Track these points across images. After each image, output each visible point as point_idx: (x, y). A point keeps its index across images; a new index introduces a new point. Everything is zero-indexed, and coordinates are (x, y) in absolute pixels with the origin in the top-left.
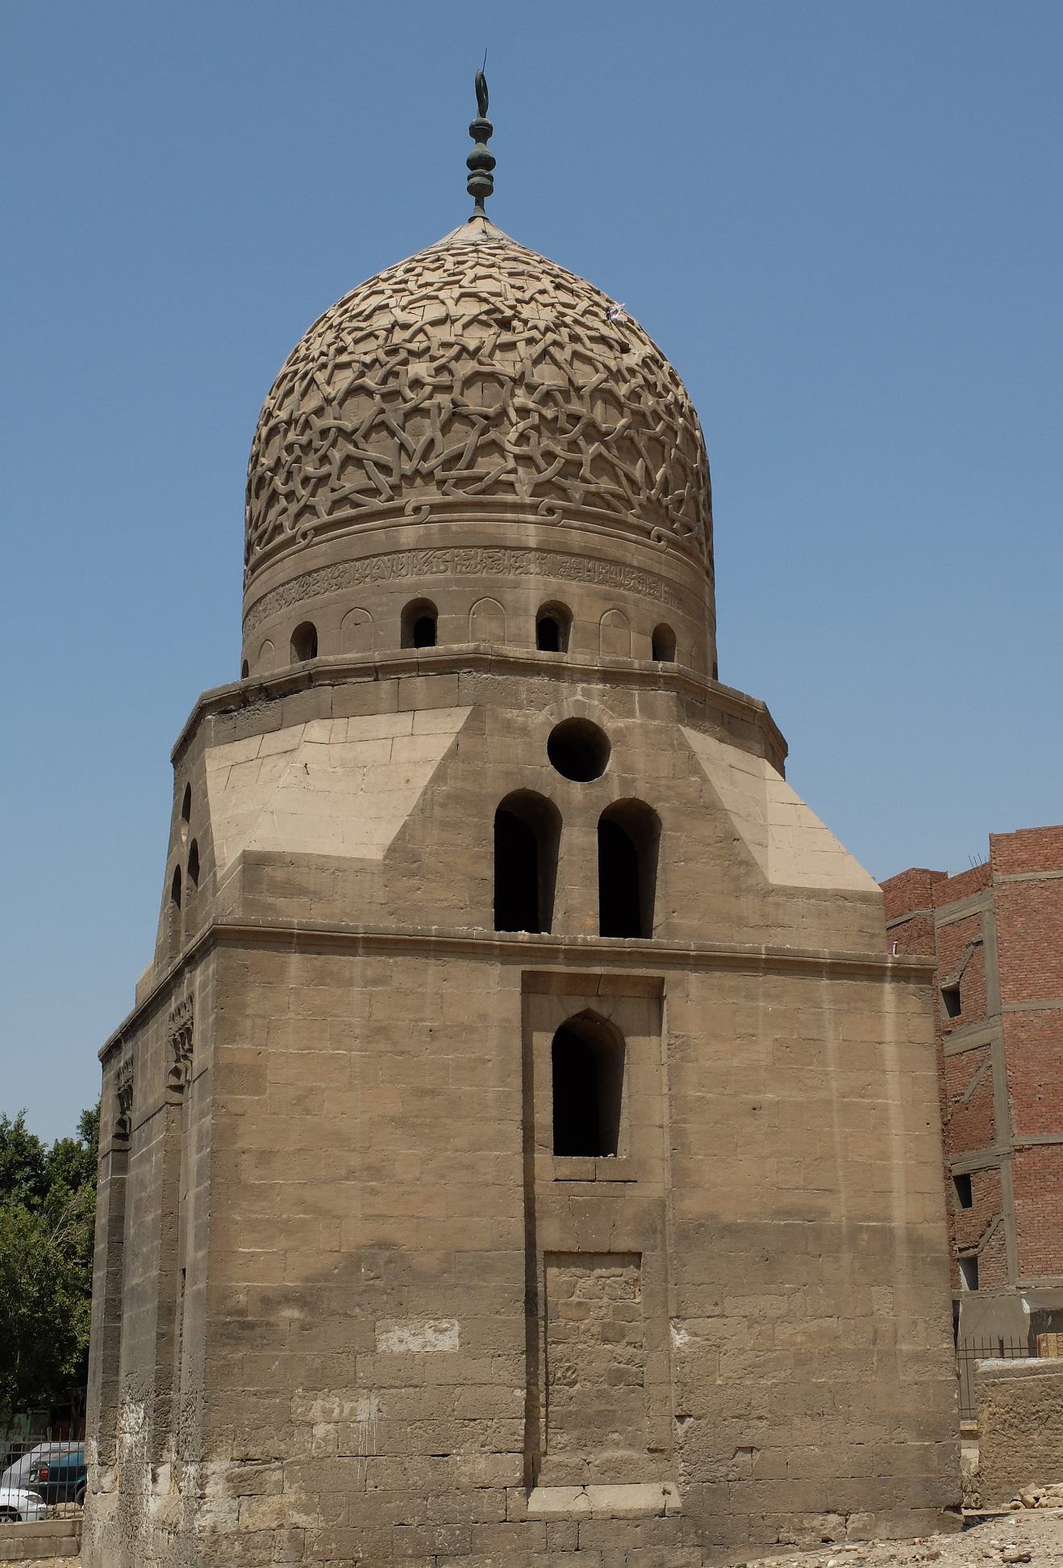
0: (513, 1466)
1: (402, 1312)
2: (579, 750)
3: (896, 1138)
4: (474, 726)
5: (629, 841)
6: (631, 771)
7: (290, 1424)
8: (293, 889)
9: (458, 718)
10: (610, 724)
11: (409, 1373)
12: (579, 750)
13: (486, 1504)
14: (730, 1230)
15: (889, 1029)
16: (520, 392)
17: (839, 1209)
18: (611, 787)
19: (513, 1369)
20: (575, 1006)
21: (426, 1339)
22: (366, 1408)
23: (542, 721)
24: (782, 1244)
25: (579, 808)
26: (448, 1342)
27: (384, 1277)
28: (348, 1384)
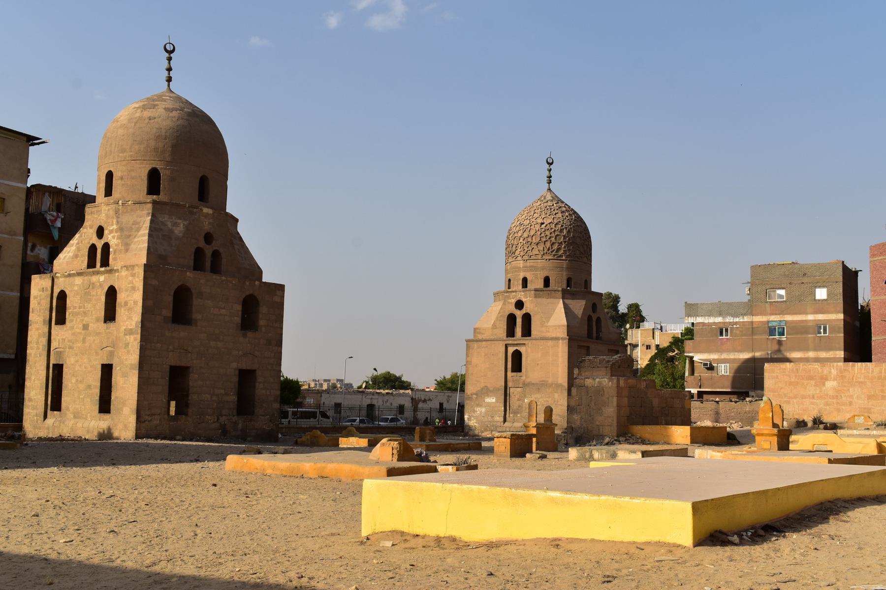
0: (502, 419)
1: (488, 396)
2: (520, 305)
3: (560, 370)
4: (504, 304)
5: (527, 318)
6: (528, 308)
7: (474, 411)
8: (479, 333)
9: (501, 303)
10: (524, 300)
11: (489, 404)
12: (520, 305)
13: (498, 424)
14: (533, 384)
15: (560, 350)
16: (80, 385)
17: (550, 381)
18: (524, 311)
19: (502, 405)
20: (515, 348)
21: (491, 400)
22: (483, 410)
23: (514, 301)
24: (541, 386)
25: (519, 314)
26: (494, 400)
27: (486, 391)
28: (481, 406)
